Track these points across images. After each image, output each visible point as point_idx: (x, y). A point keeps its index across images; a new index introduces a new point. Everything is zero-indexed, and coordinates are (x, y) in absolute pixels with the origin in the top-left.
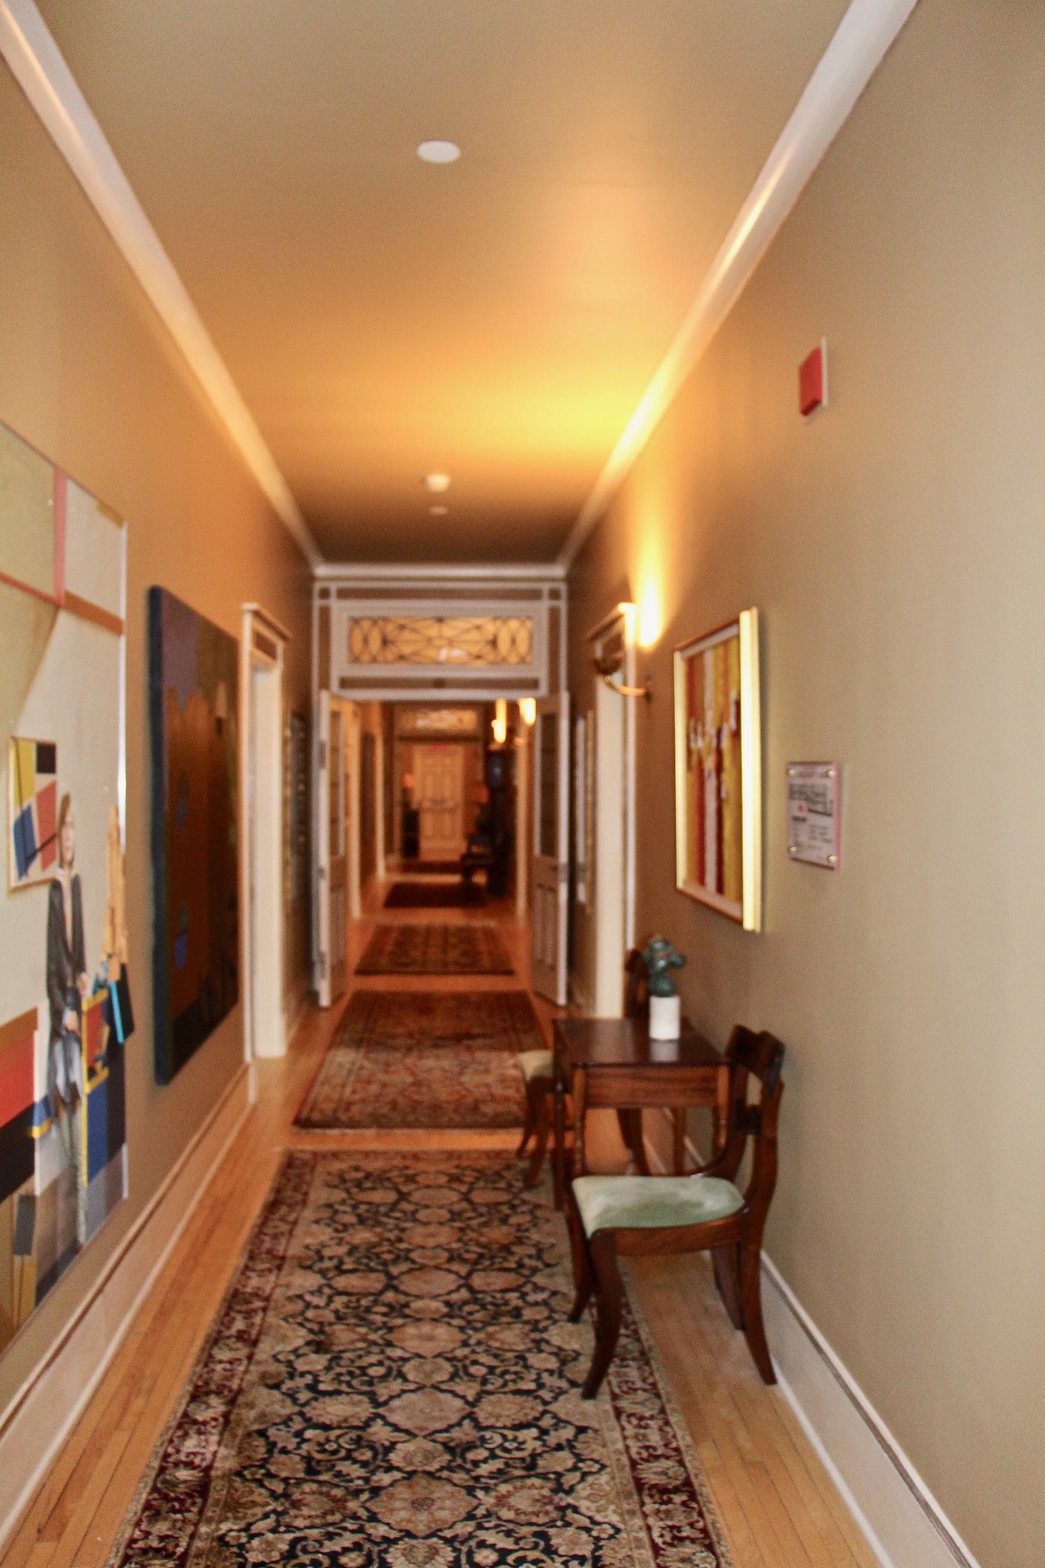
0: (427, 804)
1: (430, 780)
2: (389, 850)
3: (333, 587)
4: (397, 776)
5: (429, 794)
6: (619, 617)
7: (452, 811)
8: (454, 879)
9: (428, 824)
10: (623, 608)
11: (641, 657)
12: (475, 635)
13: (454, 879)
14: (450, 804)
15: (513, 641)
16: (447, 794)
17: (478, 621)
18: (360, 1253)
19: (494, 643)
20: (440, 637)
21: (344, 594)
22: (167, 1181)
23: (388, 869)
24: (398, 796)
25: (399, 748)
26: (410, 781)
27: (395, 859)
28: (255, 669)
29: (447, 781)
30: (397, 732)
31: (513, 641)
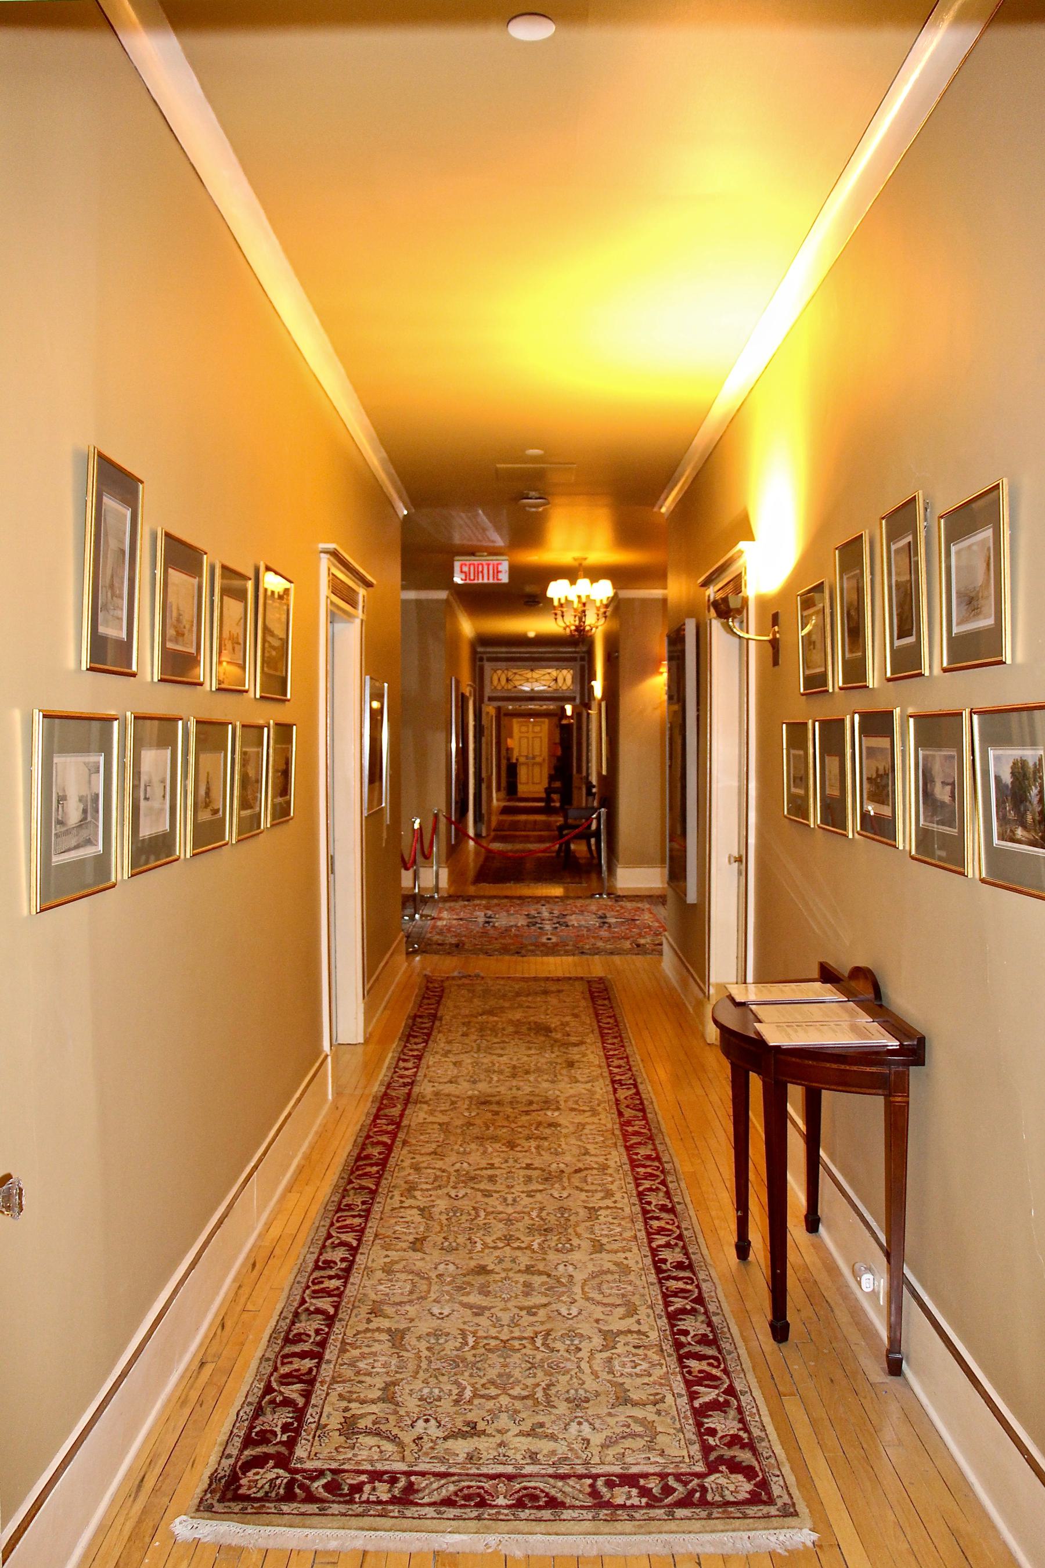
0: (522, 760)
1: (524, 741)
2: (498, 789)
3: (485, 656)
4: (502, 741)
5: (524, 753)
6: (740, 553)
7: (540, 764)
8: (542, 804)
9: (523, 773)
10: (742, 545)
11: (763, 603)
12: (547, 677)
13: (542, 804)
14: (538, 760)
15: (565, 680)
16: (537, 752)
17: (549, 671)
18: (501, 943)
19: (556, 680)
20: (532, 678)
21: (489, 660)
22: (388, 955)
23: (498, 800)
24: (503, 752)
25: (505, 721)
26: (510, 742)
27: (503, 794)
28: (332, 618)
29: (537, 743)
30: (488, 692)
31: (565, 680)
